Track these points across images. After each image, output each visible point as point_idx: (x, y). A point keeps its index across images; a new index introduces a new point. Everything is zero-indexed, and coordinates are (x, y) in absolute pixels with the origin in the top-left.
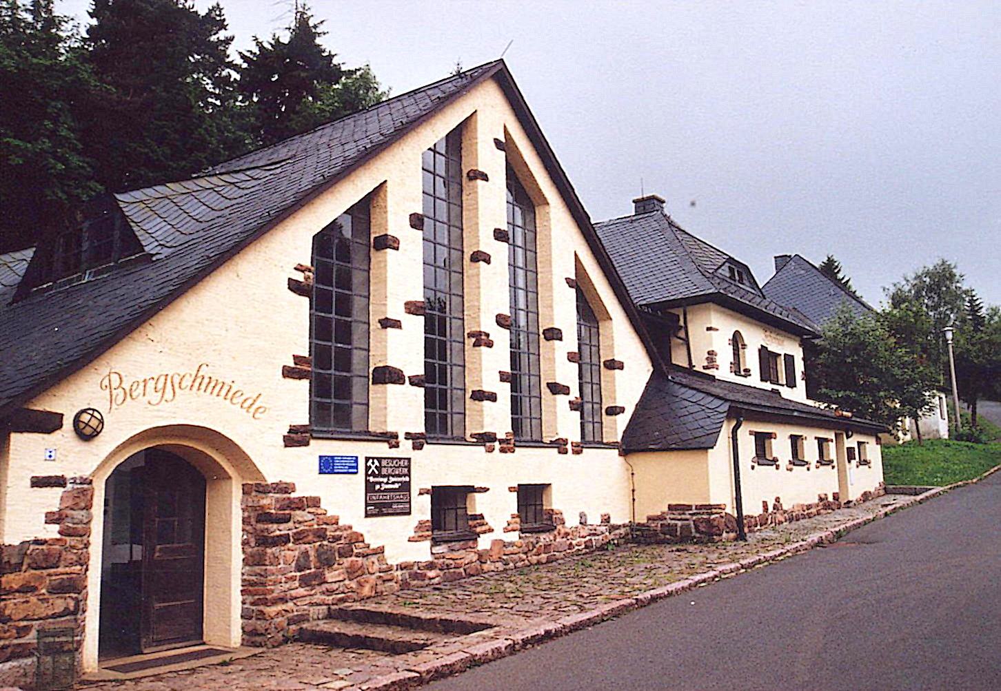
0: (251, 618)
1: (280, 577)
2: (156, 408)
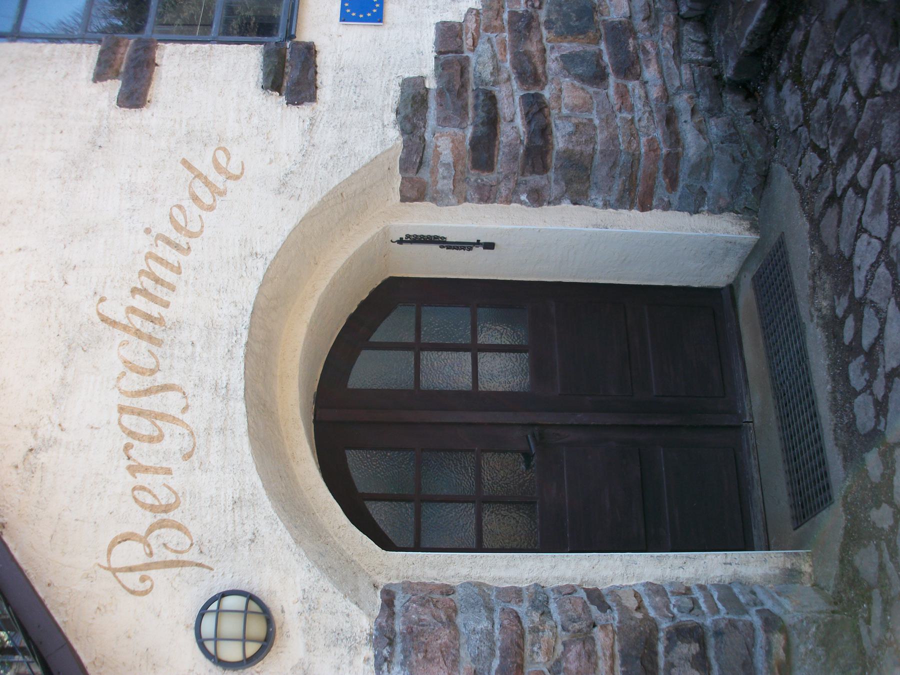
0: (703, 192)
1: (618, 122)
2: (200, 441)
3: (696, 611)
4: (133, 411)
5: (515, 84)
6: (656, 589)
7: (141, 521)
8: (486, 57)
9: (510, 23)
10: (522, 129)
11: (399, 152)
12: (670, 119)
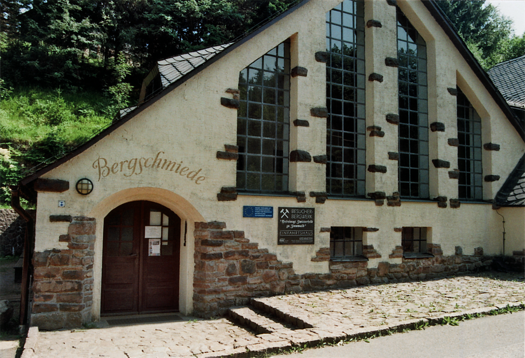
3: (85, 290)
4: (136, 162)
5: (225, 251)
6: (92, 282)
7: (110, 165)
8: (233, 244)
9: (245, 251)
10: (211, 253)
11: (204, 222)
12: (216, 292)
